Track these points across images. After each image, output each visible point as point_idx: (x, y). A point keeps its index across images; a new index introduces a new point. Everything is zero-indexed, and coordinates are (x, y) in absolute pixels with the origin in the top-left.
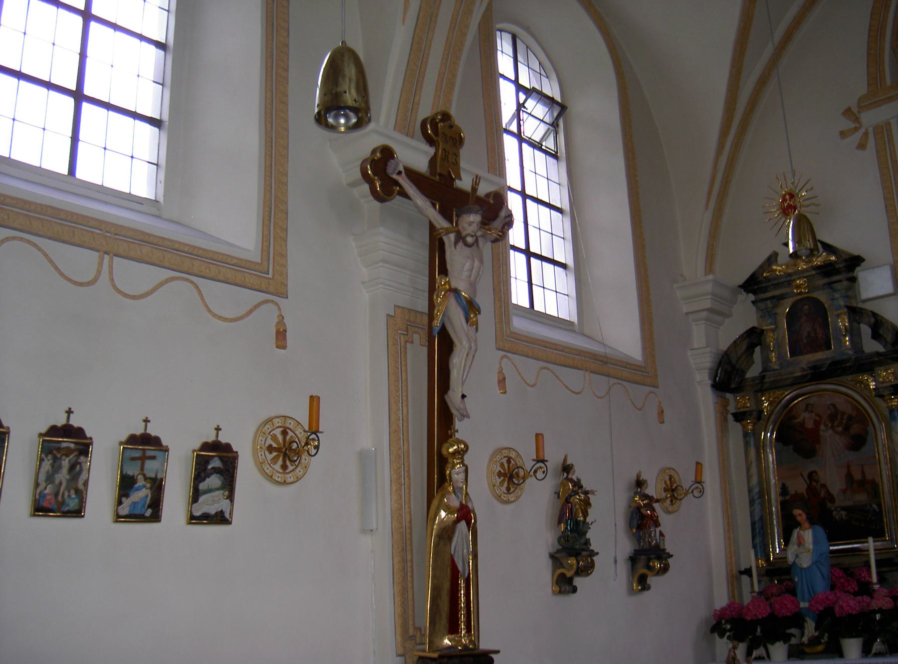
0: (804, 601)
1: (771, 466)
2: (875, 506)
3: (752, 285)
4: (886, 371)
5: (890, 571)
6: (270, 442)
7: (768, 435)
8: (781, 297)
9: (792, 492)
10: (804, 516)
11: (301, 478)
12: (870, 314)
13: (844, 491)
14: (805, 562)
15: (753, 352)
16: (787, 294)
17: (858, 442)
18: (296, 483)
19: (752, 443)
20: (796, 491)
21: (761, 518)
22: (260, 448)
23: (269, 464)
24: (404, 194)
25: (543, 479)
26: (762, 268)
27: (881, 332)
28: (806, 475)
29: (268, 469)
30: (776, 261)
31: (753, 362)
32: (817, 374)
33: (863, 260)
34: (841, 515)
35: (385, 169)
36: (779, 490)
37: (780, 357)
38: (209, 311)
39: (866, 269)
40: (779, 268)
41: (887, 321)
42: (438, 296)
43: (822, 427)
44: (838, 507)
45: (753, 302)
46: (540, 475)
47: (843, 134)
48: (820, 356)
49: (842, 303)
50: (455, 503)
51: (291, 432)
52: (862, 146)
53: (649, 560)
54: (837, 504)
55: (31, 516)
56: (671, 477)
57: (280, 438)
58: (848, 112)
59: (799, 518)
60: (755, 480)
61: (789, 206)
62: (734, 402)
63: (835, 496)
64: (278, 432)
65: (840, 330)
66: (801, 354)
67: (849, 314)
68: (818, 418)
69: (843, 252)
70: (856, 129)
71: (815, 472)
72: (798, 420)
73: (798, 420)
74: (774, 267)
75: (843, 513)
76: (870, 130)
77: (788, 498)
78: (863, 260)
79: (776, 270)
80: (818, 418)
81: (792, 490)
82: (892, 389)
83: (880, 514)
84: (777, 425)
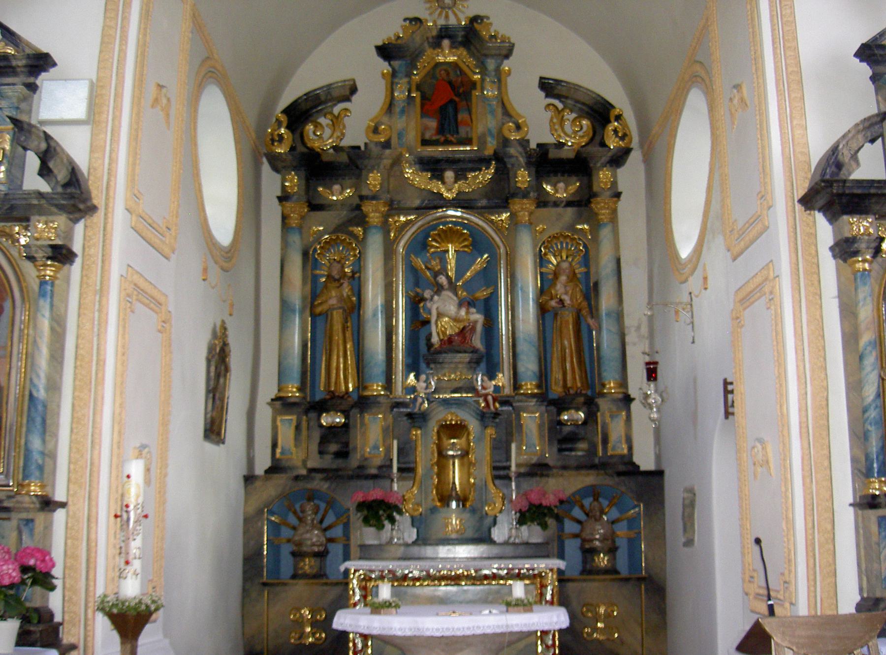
12: (42, 135)
20: (805, 211)
27: (51, 165)
33: (54, 64)
55: (541, 78)
67: (14, 134)
69: (28, 44)
78: (54, 64)
82: (49, 250)
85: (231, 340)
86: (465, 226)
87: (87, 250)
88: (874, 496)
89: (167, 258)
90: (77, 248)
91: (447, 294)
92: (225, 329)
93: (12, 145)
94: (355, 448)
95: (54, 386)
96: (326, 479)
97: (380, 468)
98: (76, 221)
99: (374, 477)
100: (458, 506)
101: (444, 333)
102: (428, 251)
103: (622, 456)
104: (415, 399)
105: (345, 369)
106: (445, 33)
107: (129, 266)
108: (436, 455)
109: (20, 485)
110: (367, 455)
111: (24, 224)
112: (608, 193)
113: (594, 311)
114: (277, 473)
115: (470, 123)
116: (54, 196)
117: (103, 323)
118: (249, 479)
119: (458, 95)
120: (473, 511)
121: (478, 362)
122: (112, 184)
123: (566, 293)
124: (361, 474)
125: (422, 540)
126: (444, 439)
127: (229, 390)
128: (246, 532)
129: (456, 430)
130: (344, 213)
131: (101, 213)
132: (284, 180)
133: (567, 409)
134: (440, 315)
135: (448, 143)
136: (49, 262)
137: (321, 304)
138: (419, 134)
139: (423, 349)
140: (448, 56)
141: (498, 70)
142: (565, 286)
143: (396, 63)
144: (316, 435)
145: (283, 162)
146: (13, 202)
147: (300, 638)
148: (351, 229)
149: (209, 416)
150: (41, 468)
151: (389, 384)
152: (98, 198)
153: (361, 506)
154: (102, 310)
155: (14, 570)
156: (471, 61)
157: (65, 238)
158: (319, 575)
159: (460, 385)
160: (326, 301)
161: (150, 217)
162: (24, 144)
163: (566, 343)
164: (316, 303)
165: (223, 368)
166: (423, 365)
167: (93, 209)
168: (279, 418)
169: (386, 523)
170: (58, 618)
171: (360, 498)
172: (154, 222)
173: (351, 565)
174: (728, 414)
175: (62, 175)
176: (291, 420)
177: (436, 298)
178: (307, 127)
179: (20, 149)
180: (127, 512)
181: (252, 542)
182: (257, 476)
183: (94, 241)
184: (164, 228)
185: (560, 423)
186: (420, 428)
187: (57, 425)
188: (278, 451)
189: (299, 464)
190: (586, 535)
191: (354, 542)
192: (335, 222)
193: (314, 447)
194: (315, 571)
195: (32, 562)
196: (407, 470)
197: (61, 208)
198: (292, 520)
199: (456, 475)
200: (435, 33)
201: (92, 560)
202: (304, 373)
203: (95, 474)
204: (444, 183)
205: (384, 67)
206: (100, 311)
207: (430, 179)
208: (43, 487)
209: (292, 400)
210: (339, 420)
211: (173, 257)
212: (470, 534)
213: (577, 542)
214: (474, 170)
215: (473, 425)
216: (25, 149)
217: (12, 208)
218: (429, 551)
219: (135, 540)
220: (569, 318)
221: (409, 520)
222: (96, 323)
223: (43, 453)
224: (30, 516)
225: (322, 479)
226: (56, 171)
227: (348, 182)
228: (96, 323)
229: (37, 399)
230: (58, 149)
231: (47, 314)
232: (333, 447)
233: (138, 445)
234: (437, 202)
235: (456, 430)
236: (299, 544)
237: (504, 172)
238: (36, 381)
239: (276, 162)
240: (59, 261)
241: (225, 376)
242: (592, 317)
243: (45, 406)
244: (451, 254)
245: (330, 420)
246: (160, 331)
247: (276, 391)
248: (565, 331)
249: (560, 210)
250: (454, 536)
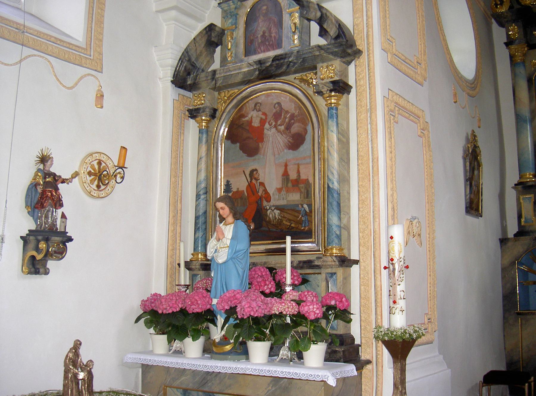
2: (305, 206)
5: (314, 274)
6: (90, 169)
9: (234, 189)
10: (227, 210)
11: (110, 194)
13: (279, 190)
15: (214, 51)
18: (107, 197)
19: (204, 140)
21: (205, 213)
22: (84, 173)
23: (88, 184)
25: (120, 183)
27: (325, 26)
28: (247, 173)
29: (88, 187)
31: (214, 62)
34: (275, 214)
38: (6, 64)
43: (267, 126)
44: (273, 206)
51: (104, 163)
54: (273, 202)
57: (96, 167)
60: (203, 175)
63: (271, 195)
64: (95, 163)
68: (264, 117)
71: (256, 170)
72: (246, 119)
73: (246, 119)
75: (277, 212)
77: (230, 194)
80: (264, 117)
83: (309, 214)
85: (480, 144)
87: (358, 82)
89: (421, 85)
90: (351, 82)
92: (475, 136)
93: (300, 20)
95: (345, 180)
98: (349, 63)
107: (389, 89)
109: (326, 250)
111: (314, 72)
114: (522, 236)
116: (329, 47)
117: (375, 131)
118: (503, 241)
122: (370, 33)
127: (482, 179)
128: (503, 278)
131: (365, 55)
132: (508, 31)
136: (333, 94)
145: (505, 18)
146: (304, 56)
149: (468, 197)
150: (339, 237)
152: (360, 44)
154: (373, 122)
155: (318, 308)
157: (341, 76)
161: (403, 55)
162: (307, 16)
165: (476, 163)
167: (358, 53)
170: (357, 342)
172: (406, 58)
175: (333, 31)
176: (531, 197)
179: (306, 21)
180: (392, 264)
181: (508, 285)
182: (509, 238)
183: (363, 75)
184: (415, 63)
187: (349, 207)
188: (523, 220)
195: (333, 303)
197: (335, 54)
201: (379, 300)
203: (377, 240)
206: (371, 124)
208: (341, 249)
209: (530, 184)
211: (426, 84)
216: (309, 20)
217: (304, 60)
219: (399, 285)
222: (369, 132)
223: (339, 227)
224: (334, 271)
226: (329, 30)
228: (369, 132)
229: (333, 189)
230: (328, 14)
231: (335, 129)
233: (409, 217)
238: (331, 177)
240: (339, 92)
241: (479, 169)
243: (339, 194)
246: (420, 136)
247: (518, 179)
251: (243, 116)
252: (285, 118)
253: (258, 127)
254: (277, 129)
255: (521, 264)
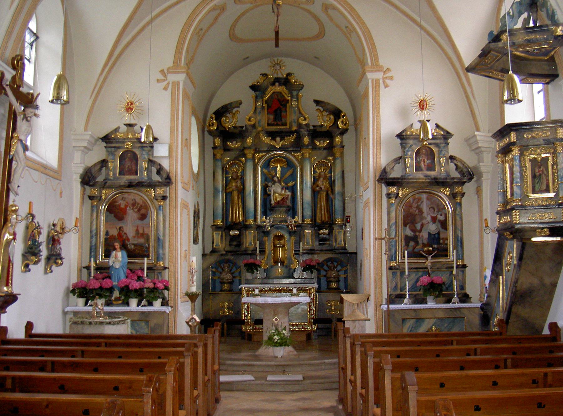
0: (115, 281)
1: (102, 222)
2: (147, 245)
3: (106, 139)
4: (161, 189)
7: (103, 207)
8: (119, 148)
13: (134, 237)
14: (117, 266)
16: (121, 147)
17: (143, 217)
19: (95, 210)
24: (6, 94)
26: (112, 133)
28: (118, 228)
30: (119, 131)
32: (130, 185)
35: (2, 83)
36: (105, 233)
37: (114, 174)
39: (158, 143)
40: (119, 134)
41: (165, 169)
42: (13, 142)
43: (128, 208)
45: (105, 147)
46: (74, 231)
47: (158, 81)
48: (133, 177)
49: (146, 157)
50: (12, 232)
52: (165, 89)
53: (57, 259)
56: (63, 223)
58: (162, 71)
59: (116, 247)
61: (130, 108)
62: (90, 191)
65: (143, 168)
66: (124, 175)
68: (127, 204)
70: (164, 80)
72: (118, 203)
73: (118, 203)
74: (117, 134)
75: (133, 246)
76: (171, 83)
79: (118, 135)
81: (111, 234)
83: (148, 248)
84: (108, 204)
86: (284, 158)
88: (391, 266)
90: (168, 195)
91: (277, 184)
94: (243, 244)
95: (164, 235)
96: (232, 255)
97: (253, 251)
99: (250, 254)
100: (281, 265)
101: (276, 200)
102: (270, 167)
103: (343, 247)
104: (265, 226)
105: (239, 213)
106: (277, 80)
108: (273, 246)
110: (247, 246)
112: (339, 146)
113: (333, 192)
115: (286, 117)
118: (204, 255)
119: (281, 105)
120: (286, 267)
121: (289, 210)
123: (323, 185)
124: (245, 253)
125: (268, 277)
126: (276, 241)
129: (281, 237)
130: (237, 153)
133: (322, 229)
134: (274, 193)
135: (277, 125)
137: (229, 188)
138: (266, 121)
139: (268, 206)
140: (278, 88)
141: (297, 95)
142: (322, 182)
143: (257, 93)
144: (228, 239)
147: (224, 313)
148: (240, 159)
150: (162, 258)
151: (255, 219)
153: (246, 265)
156: (287, 92)
158: (230, 290)
159: (282, 219)
160: (231, 187)
163: (322, 203)
164: (227, 188)
166: (268, 211)
168: (214, 233)
169: (255, 271)
170: (167, 299)
171: (245, 262)
173: (243, 286)
174: (362, 239)
175: (165, 176)
177: (273, 186)
178: (222, 119)
185: (319, 234)
186: (267, 237)
189: (222, 249)
190: (328, 275)
191: (243, 279)
192: (234, 156)
193: (228, 243)
194: (229, 289)
196: (262, 252)
198: (220, 270)
199: (281, 254)
200: (272, 80)
202: (223, 215)
204: (276, 142)
205: (253, 93)
207: (271, 140)
210: (237, 232)
212: (285, 275)
213: (325, 278)
214: (287, 137)
215: (286, 236)
218: (270, 281)
220: (324, 194)
221: (263, 270)
225: (231, 255)
227: (239, 140)
231: (161, 215)
232: (235, 243)
234: (274, 148)
235: (281, 237)
236: (223, 279)
237: (299, 138)
239: (210, 132)
242: (332, 195)
243: (163, 241)
244: (279, 169)
245: (233, 233)
248: (322, 199)
249: (321, 151)
250: (279, 275)
251: (116, 202)
252: (137, 206)
253: (123, 208)
254: (133, 211)
255: (212, 268)
